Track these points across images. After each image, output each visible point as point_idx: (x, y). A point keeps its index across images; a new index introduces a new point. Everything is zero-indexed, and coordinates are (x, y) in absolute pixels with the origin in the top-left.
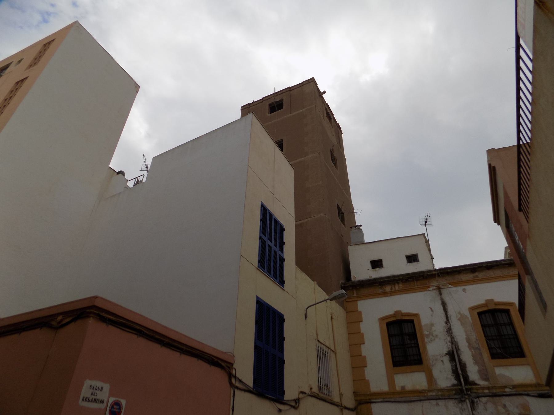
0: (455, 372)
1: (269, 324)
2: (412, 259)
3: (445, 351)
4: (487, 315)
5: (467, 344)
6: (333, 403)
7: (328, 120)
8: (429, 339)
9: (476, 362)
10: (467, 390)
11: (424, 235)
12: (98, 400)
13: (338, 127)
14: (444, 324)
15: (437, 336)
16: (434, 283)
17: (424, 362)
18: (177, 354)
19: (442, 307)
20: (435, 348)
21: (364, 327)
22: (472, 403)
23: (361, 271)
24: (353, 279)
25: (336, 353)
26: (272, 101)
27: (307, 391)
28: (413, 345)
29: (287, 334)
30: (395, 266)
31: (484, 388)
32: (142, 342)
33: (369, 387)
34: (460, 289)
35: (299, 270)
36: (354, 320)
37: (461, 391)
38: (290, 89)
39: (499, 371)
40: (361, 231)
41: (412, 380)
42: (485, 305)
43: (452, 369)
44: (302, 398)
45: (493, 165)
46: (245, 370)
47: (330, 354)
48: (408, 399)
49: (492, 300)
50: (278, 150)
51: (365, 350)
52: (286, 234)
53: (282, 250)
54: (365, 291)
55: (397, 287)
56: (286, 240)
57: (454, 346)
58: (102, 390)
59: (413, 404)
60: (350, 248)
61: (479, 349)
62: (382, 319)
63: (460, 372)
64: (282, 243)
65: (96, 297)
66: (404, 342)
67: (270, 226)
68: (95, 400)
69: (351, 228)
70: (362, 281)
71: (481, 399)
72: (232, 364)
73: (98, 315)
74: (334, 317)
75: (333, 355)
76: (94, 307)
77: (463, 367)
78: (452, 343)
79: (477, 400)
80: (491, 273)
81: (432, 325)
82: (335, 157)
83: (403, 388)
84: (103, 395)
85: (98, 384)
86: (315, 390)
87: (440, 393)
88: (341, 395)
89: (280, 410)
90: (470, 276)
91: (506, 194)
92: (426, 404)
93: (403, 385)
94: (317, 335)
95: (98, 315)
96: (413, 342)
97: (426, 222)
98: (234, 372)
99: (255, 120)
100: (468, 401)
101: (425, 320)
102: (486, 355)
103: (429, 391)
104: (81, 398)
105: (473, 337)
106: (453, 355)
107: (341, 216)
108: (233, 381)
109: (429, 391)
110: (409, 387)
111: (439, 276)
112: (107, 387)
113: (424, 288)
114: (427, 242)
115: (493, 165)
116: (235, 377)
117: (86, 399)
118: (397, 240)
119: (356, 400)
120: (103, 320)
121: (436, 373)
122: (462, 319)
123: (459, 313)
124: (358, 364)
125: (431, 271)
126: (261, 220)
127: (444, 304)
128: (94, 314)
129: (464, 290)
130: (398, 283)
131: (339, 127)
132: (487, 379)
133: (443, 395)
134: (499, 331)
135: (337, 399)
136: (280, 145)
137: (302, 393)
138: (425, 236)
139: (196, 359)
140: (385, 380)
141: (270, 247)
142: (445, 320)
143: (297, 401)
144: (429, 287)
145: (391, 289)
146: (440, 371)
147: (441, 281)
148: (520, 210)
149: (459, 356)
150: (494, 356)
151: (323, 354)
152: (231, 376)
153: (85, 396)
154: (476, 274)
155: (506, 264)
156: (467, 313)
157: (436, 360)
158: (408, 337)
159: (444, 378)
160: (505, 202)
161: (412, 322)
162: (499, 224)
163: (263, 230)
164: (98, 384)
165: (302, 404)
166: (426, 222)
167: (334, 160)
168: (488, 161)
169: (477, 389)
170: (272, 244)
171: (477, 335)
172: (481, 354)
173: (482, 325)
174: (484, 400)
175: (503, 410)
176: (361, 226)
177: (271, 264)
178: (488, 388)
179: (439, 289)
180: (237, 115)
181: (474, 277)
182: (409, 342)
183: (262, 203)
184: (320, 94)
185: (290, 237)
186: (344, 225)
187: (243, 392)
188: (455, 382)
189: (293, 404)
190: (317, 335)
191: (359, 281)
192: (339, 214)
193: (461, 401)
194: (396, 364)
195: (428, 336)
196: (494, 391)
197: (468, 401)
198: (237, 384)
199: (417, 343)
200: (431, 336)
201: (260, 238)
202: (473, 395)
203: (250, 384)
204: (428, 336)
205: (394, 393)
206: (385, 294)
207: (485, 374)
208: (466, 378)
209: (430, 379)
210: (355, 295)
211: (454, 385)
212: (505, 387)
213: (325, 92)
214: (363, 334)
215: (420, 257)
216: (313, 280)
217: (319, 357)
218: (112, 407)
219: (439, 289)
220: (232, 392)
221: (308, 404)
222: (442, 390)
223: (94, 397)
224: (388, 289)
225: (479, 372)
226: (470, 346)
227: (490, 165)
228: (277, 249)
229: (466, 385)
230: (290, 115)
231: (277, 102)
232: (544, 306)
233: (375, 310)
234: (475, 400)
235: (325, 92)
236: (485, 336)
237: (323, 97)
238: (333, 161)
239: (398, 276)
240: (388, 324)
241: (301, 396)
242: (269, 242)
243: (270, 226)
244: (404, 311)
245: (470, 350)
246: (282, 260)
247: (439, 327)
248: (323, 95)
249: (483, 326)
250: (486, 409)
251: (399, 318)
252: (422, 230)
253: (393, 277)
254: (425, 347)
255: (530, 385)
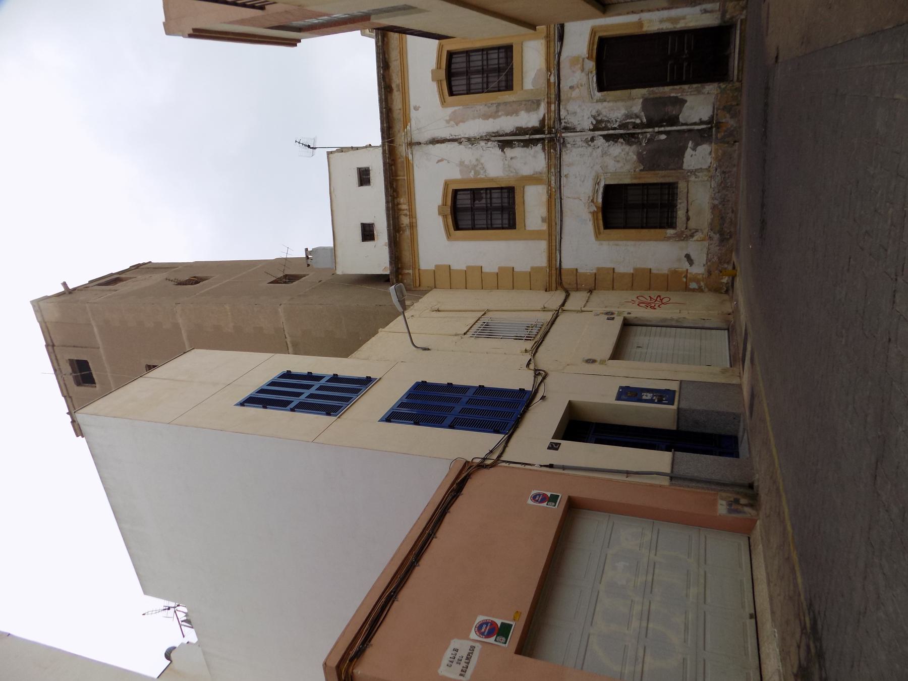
0: (527, 144)
1: (427, 405)
2: (364, 177)
3: (498, 151)
4: (453, 83)
5: (491, 120)
6: (553, 322)
7: (122, 283)
8: (482, 172)
9: (516, 112)
10: (550, 133)
11: (329, 153)
12: (469, 654)
13: (137, 268)
14: (462, 147)
15: (477, 160)
16: (402, 150)
17: (511, 184)
18: (435, 542)
19: (438, 145)
20: (494, 166)
21: (459, 265)
22: (567, 129)
23: (375, 258)
24: (388, 272)
25: (488, 311)
26: (70, 380)
27: (528, 357)
28: (489, 196)
29: (444, 381)
30: (372, 204)
31: (549, 111)
32: (406, 594)
33: (541, 268)
34: (413, 114)
35: (356, 354)
36: (447, 278)
37: (551, 140)
38: (51, 346)
39: (528, 85)
40: (315, 251)
41: (533, 205)
42: (439, 82)
43: (523, 147)
44: (535, 366)
45: (191, 32)
46: (476, 444)
47: (485, 319)
48: (558, 215)
49: (433, 71)
50: (154, 373)
51: (491, 267)
52: (296, 370)
53: (319, 378)
54: (406, 256)
55: (404, 207)
56: (304, 370)
57: (493, 139)
58: (457, 650)
59: (564, 209)
60: (339, 272)
61: (499, 104)
62: (449, 236)
63: (527, 137)
64: (310, 376)
65: (325, 664)
66: (479, 209)
67: (276, 395)
68: (467, 658)
69: (308, 265)
70: (391, 258)
71: (562, 117)
72: (467, 462)
73: (351, 660)
74: (436, 308)
75: (490, 315)
76: (338, 667)
77: (520, 131)
78: (488, 140)
79: (563, 121)
80: (395, 65)
81: (462, 164)
82: (191, 278)
83: (543, 220)
84: (462, 646)
85: (448, 654)
86: (529, 345)
87: (553, 170)
88: (544, 309)
89: (543, 398)
90: (397, 96)
91: (242, 22)
92: (566, 192)
93: (540, 221)
94: (456, 335)
95: (351, 660)
96: (484, 195)
97: (309, 146)
98: (478, 461)
99: (90, 409)
100: (563, 135)
101: (455, 174)
102: (506, 97)
103: (550, 185)
104: (461, 678)
105: (482, 109)
106: (505, 142)
107: (290, 279)
108: (488, 462)
109: (550, 185)
110: (543, 211)
111: (392, 142)
112: (455, 643)
113: (409, 166)
114: (342, 150)
115: (191, 32)
116: (484, 459)
117: (463, 672)
118: (333, 197)
119: (556, 289)
120: (360, 653)
121: (526, 171)
122: (456, 120)
123: (448, 122)
124: (507, 279)
125: (384, 152)
126: (265, 407)
127: (434, 141)
128: (349, 666)
129: (416, 108)
130: (398, 204)
131: (137, 266)
132: (538, 103)
133: (556, 165)
134: (474, 73)
135: (549, 316)
136: (150, 368)
137: (528, 365)
138: (331, 152)
139: (448, 515)
140: (531, 243)
141: (311, 396)
142: (456, 144)
143: (537, 372)
144: (407, 158)
145: (406, 215)
146: (525, 164)
147: (401, 140)
148: (262, 8)
149: (507, 135)
150: (509, 87)
151: (486, 330)
152: (481, 466)
153: (460, 672)
154: (394, 86)
155: (383, 41)
156: (450, 110)
157: (509, 167)
158: (477, 202)
159: (531, 160)
160: (254, 26)
161: (456, 192)
162: (299, 41)
163: (282, 405)
164: (448, 654)
165: (541, 366)
166: (309, 146)
167: (195, 281)
168: (184, 36)
169: (550, 119)
170: (307, 392)
171: (480, 102)
172: (505, 103)
173: (467, 94)
174: (563, 113)
175: (577, 90)
176: (306, 250)
177: (332, 397)
178: (549, 103)
179: (411, 144)
180: (82, 440)
181: (399, 90)
182: (484, 201)
183: (237, 405)
184: (68, 292)
185: (301, 364)
186: (304, 276)
187: (507, 449)
188: (540, 146)
189: (540, 378)
190: (456, 335)
191: (391, 263)
192: (285, 283)
193: (564, 144)
194: (512, 225)
195: (477, 173)
196: (553, 96)
197: (563, 135)
198: (495, 457)
199: (487, 189)
200: (477, 168)
201: (292, 410)
202: (557, 126)
203: (498, 437)
204: (477, 173)
205: (550, 235)
206: (413, 226)
207: (532, 105)
208: (535, 131)
209: (534, 179)
210: (411, 271)
211: (544, 149)
212: (549, 80)
213: (64, 284)
214: (468, 267)
215: (363, 165)
216: (375, 333)
217: (490, 336)
218: (482, 634)
219: (411, 144)
220: (504, 464)
221: (544, 359)
222: (549, 167)
223: (464, 660)
224: (405, 221)
225: (528, 110)
226: (494, 115)
227: (190, 36)
228: (317, 384)
229: (543, 133)
230: (102, 351)
231: (74, 371)
232: (407, 9)
233: (436, 244)
234: (563, 124)
235: (64, 284)
236: (483, 92)
237: (75, 289)
238: (197, 283)
239: (387, 202)
240: (457, 227)
241: (532, 366)
242: (303, 397)
243: (276, 395)
244: (439, 201)
245: (499, 116)
246: (335, 378)
247: (465, 153)
248: (71, 287)
249: (469, 92)
250: (575, 113)
251: (448, 210)
252: (321, 155)
253: (388, 209)
254: (492, 180)
255: (548, 47)
